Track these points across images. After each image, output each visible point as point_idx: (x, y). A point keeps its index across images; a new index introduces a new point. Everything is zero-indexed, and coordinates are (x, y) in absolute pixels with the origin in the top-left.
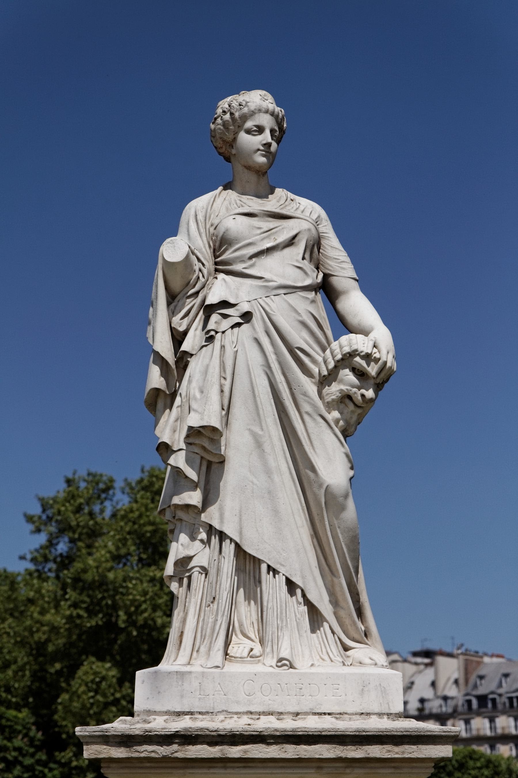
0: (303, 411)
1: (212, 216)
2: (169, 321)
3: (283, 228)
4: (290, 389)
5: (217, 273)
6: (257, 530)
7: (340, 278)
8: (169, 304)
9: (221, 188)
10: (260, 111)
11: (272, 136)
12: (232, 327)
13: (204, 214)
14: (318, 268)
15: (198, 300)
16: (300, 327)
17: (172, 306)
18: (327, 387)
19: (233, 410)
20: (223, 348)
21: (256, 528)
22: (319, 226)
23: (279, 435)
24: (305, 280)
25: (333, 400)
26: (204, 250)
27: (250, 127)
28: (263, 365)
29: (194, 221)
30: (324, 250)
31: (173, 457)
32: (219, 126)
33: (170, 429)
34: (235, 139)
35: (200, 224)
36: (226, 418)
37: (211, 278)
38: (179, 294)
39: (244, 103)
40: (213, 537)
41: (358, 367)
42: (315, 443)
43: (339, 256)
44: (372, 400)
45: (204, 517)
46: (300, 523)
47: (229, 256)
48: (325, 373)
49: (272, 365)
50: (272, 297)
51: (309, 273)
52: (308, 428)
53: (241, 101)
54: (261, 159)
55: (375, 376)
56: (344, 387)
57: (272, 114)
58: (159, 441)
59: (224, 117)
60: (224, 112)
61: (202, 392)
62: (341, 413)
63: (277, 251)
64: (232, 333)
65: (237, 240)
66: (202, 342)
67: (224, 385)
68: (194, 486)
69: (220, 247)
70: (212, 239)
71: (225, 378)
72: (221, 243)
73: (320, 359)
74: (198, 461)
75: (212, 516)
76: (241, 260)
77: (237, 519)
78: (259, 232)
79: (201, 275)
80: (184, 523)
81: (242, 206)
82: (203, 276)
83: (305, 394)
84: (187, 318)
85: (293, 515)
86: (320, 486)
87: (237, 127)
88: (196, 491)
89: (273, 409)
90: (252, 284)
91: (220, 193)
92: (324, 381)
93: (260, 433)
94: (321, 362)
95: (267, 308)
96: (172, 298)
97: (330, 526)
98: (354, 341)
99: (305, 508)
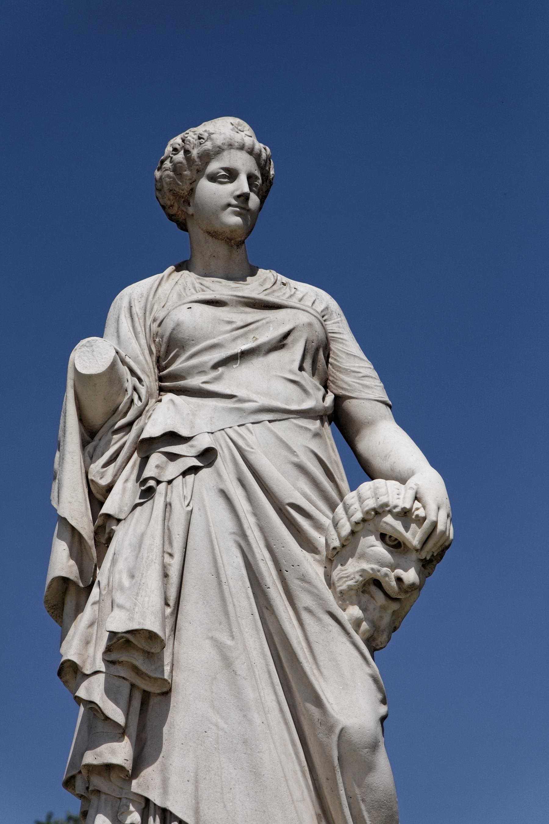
0: (300, 605)
1: (156, 307)
2: (84, 471)
3: (267, 323)
4: (279, 570)
5: (162, 393)
6: (225, 806)
7: (363, 401)
8: (84, 444)
9: (172, 268)
10: (231, 146)
11: (250, 185)
12: (184, 474)
13: (142, 304)
14: (326, 387)
15: (130, 437)
16: (295, 473)
17: (90, 447)
18: (339, 567)
19: (186, 607)
20: (168, 506)
21: (223, 802)
22: (327, 323)
23: (262, 648)
24: (303, 401)
25: (350, 588)
26: (141, 358)
27: (216, 172)
28: (234, 533)
29: (128, 315)
30: (335, 360)
31: (85, 684)
32: (168, 172)
33: (83, 643)
34: (192, 191)
35: (136, 319)
36: (173, 620)
37: (152, 401)
38: (100, 429)
39: (205, 135)
40: (151, 819)
41: (388, 531)
42: (321, 658)
43: (359, 367)
44: (413, 586)
45: (135, 786)
46: (297, 795)
47: (180, 366)
48: (336, 543)
49: (249, 533)
50: (250, 426)
51: (311, 391)
52: (309, 634)
53: (201, 132)
54: (233, 220)
55: (419, 547)
56: (367, 566)
57: (251, 152)
58: (62, 660)
59: (175, 157)
60: (175, 150)
61: (132, 577)
62: (364, 610)
63: (258, 355)
64: (184, 484)
65: (194, 341)
66: (134, 500)
67: (170, 565)
68: (120, 732)
69: (167, 352)
70: (154, 341)
71: (171, 555)
72: (168, 348)
73: (327, 522)
74: (126, 691)
75: (148, 784)
76: (200, 370)
77: (190, 788)
78: (229, 327)
79: (136, 397)
80: (103, 797)
81: (203, 291)
82: (140, 398)
83: (304, 579)
84: (113, 465)
85: (287, 781)
86: (330, 729)
87: (195, 172)
88: (122, 741)
89: (250, 604)
90: (216, 406)
91: (170, 274)
92: (336, 557)
93: (229, 642)
94: (329, 527)
95: (241, 443)
96: (90, 435)
97: (349, 797)
98: (382, 490)
99: (307, 768)
